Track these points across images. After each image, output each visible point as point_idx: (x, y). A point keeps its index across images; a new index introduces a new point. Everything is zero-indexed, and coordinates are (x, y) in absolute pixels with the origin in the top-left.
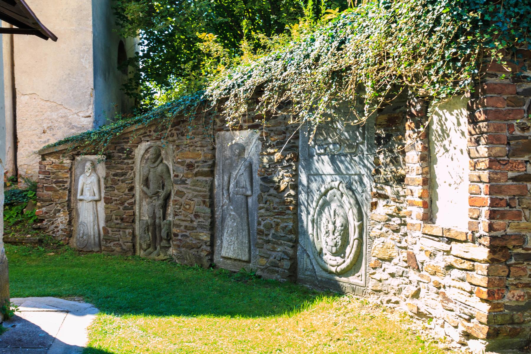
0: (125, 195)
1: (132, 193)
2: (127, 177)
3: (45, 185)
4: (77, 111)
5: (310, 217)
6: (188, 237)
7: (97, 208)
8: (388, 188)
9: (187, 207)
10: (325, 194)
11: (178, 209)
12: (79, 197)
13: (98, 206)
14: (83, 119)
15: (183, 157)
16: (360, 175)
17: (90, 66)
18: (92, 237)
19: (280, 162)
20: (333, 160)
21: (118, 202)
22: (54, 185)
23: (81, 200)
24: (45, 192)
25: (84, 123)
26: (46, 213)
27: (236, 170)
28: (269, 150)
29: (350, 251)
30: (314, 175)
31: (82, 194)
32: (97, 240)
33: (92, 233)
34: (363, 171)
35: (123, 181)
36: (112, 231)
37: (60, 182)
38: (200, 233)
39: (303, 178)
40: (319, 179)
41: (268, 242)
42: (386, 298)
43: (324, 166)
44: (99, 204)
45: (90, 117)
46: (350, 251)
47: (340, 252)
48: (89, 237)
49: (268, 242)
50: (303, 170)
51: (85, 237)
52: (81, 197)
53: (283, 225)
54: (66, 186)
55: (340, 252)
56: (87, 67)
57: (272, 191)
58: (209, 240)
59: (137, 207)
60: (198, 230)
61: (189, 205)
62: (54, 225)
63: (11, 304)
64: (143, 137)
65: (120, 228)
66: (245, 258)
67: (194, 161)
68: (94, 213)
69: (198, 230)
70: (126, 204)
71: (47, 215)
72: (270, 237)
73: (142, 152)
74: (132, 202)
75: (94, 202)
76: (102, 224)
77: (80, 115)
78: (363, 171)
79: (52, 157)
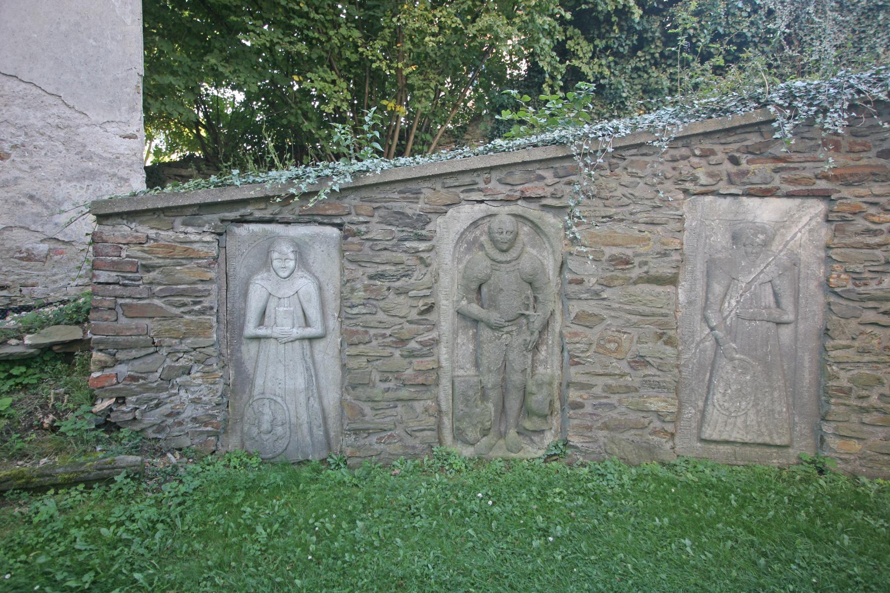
0: (411, 322)
1: (431, 317)
2: (412, 281)
3: (120, 301)
4: (101, 120)
6: (615, 407)
7: (312, 356)
9: (612, 346)
11: (583, 352)
12: (251, 329)
13: (316, 352)
14: (118, 140)
15: (597, 243)
17: (133, 21)
18: (305, 427)
21: (389, 340)
22: (157, 302)
23: (258, 338)
24: (123, 320)
25: (122, 150)
26: (133, 379)
27: (750, 273)
31: (261, 322)
32: (319, 433)
33: (304, 418)
35: (400, 292)
36: (373, 409)
37: (181, 294)
38: (649, 397)
44: (319, 346)
45: (135, 137)
48: (293, 428)
50: (609, 274)
51: (279, 430)
52: (262, 332)
54: (206, 304)
56: (129, 21)
59: (443, 352)
61: (615, 342)
62: (165, 409)
64: (462, 192)
65: (398, 400)
66: (785, 440)
67: (629, 252)
68: (307, 369)
69: (643, 391)
70: (413, 345)
71: (134, 386)
73: (460, 226)
74: (433, 339)
75: (306, 343)
76: (332, 397)
77: (109, 129)
79: (141, 223)
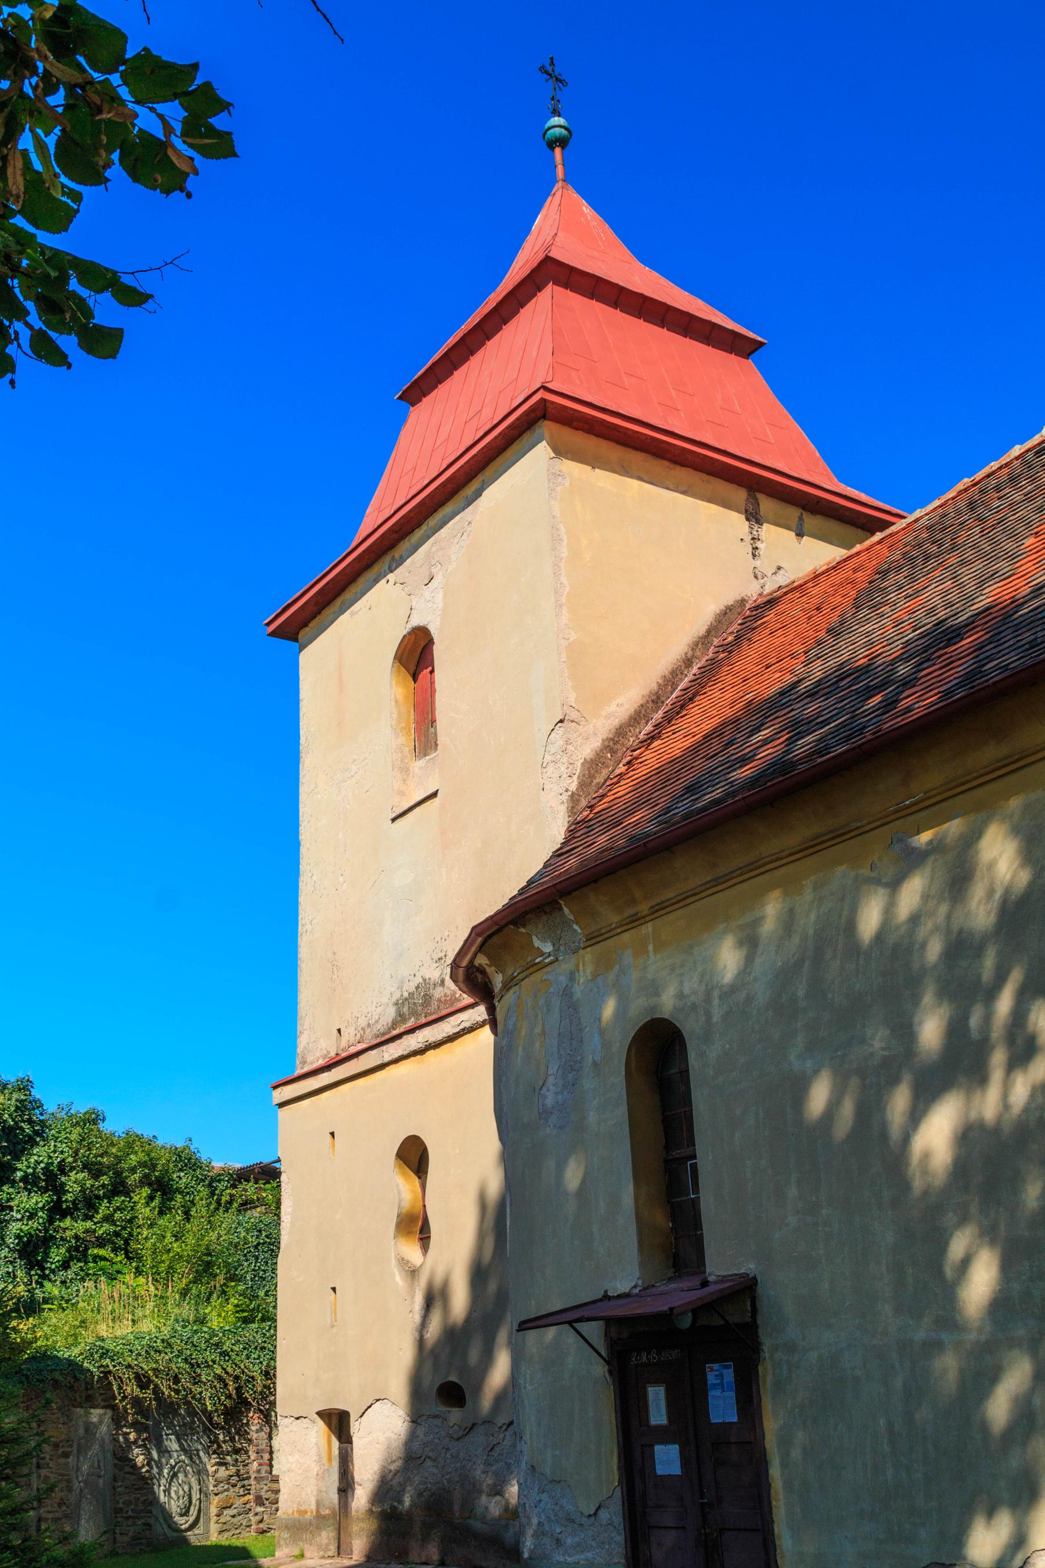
5: (162, 1488)
8: (228, 1458)
10: (174, 1467)
16: (198, 1450)
19: (135, 1442)
20: (178, 1440)
28: (124, 1430)
29: (194, 1512)
30: (164, 1451)
34: (200, 1447)
39: (155, 1455)
40: (166, 1455)
41: (127, 1518)
42: (231, 1533)
43: (173, 1445)
46: (194, 1512)
47: (186, 1513)
49: (127, 1518)
53: (142, 1499)
55: (186, 1513)
57: (127, 1469)
58: (711, 1393)
60: (63, 1520)
63: (331, 1521)
69: (63, 1520)
72: (130, 1513)
78: (200, 1447)
